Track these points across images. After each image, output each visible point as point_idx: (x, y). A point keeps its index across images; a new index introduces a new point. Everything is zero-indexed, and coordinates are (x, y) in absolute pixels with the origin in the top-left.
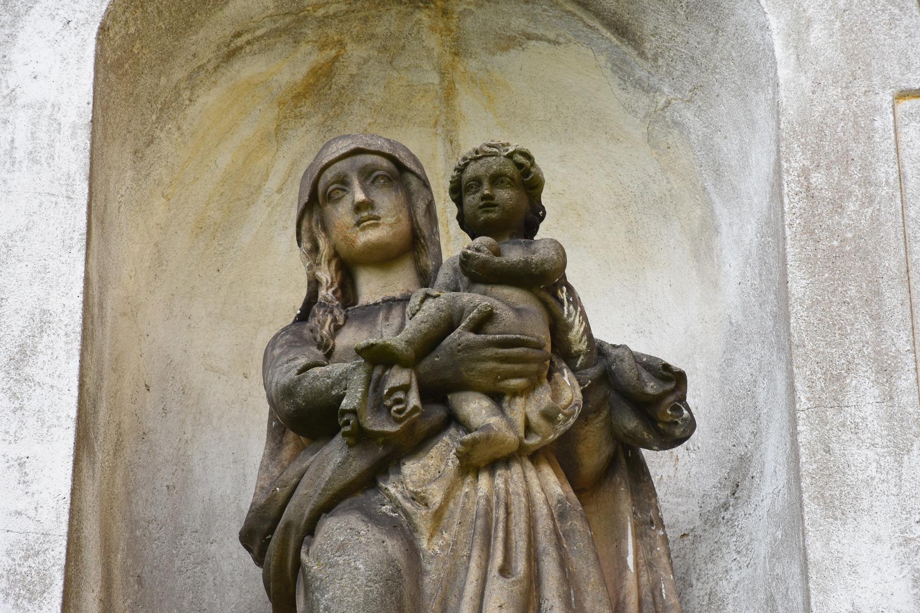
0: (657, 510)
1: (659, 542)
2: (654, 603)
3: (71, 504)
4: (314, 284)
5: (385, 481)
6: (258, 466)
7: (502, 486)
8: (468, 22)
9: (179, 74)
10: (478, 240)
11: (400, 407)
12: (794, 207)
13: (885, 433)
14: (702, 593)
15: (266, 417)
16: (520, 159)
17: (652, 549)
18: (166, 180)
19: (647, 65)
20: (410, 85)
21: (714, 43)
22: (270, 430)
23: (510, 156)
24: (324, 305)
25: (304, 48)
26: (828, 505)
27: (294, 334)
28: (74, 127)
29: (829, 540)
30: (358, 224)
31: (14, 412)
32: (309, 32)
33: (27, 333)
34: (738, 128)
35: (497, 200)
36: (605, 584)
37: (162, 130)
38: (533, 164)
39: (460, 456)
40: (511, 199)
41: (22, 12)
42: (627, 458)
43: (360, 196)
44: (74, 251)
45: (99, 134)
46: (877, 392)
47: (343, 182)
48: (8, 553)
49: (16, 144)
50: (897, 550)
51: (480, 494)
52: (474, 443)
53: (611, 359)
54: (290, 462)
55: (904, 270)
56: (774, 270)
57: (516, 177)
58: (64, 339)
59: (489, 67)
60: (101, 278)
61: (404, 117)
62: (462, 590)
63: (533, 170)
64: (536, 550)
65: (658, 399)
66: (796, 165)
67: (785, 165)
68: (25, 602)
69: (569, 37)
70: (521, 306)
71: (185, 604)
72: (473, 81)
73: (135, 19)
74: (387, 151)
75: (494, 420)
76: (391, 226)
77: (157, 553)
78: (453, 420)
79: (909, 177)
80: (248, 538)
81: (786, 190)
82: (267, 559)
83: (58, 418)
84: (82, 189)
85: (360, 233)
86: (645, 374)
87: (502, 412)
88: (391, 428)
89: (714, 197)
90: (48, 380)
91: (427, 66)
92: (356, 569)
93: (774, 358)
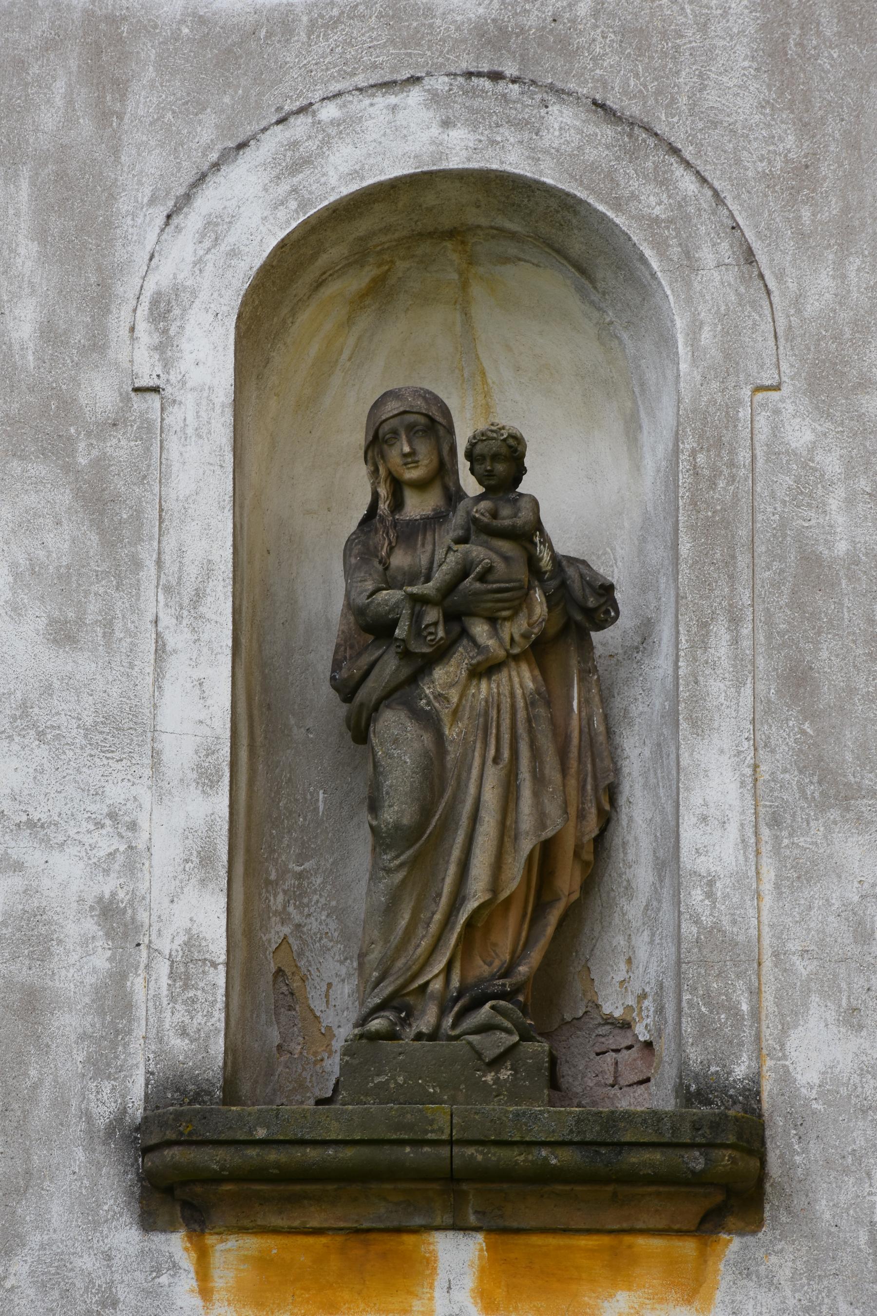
1: (594, 686)
7: (495, 690)
12: (685, 482)
13: (731, 669)
16: (511, 442)
17: (589, 691)
23: (505, 440)
26: (694, 724)
28: (223, 406)
29: (693, 751)
31: (194, 643)
33: (200, 579)
41: (187, 306)
44: (226, 510)
46: (728, 637)
47: (395, 433)
48: (196, 752)
49: (187, 422)
50: (733, 759)
58: (222, 583)
65: (595, 610)
66: (687, 446)
67: (681, 446)
70: (510, 554)
74: (424, 411)
78: (464, 633)
79: (759, 458)
84: (229, 458)
85: (406, 471)
88: (426, 650)
90: (214, 617)
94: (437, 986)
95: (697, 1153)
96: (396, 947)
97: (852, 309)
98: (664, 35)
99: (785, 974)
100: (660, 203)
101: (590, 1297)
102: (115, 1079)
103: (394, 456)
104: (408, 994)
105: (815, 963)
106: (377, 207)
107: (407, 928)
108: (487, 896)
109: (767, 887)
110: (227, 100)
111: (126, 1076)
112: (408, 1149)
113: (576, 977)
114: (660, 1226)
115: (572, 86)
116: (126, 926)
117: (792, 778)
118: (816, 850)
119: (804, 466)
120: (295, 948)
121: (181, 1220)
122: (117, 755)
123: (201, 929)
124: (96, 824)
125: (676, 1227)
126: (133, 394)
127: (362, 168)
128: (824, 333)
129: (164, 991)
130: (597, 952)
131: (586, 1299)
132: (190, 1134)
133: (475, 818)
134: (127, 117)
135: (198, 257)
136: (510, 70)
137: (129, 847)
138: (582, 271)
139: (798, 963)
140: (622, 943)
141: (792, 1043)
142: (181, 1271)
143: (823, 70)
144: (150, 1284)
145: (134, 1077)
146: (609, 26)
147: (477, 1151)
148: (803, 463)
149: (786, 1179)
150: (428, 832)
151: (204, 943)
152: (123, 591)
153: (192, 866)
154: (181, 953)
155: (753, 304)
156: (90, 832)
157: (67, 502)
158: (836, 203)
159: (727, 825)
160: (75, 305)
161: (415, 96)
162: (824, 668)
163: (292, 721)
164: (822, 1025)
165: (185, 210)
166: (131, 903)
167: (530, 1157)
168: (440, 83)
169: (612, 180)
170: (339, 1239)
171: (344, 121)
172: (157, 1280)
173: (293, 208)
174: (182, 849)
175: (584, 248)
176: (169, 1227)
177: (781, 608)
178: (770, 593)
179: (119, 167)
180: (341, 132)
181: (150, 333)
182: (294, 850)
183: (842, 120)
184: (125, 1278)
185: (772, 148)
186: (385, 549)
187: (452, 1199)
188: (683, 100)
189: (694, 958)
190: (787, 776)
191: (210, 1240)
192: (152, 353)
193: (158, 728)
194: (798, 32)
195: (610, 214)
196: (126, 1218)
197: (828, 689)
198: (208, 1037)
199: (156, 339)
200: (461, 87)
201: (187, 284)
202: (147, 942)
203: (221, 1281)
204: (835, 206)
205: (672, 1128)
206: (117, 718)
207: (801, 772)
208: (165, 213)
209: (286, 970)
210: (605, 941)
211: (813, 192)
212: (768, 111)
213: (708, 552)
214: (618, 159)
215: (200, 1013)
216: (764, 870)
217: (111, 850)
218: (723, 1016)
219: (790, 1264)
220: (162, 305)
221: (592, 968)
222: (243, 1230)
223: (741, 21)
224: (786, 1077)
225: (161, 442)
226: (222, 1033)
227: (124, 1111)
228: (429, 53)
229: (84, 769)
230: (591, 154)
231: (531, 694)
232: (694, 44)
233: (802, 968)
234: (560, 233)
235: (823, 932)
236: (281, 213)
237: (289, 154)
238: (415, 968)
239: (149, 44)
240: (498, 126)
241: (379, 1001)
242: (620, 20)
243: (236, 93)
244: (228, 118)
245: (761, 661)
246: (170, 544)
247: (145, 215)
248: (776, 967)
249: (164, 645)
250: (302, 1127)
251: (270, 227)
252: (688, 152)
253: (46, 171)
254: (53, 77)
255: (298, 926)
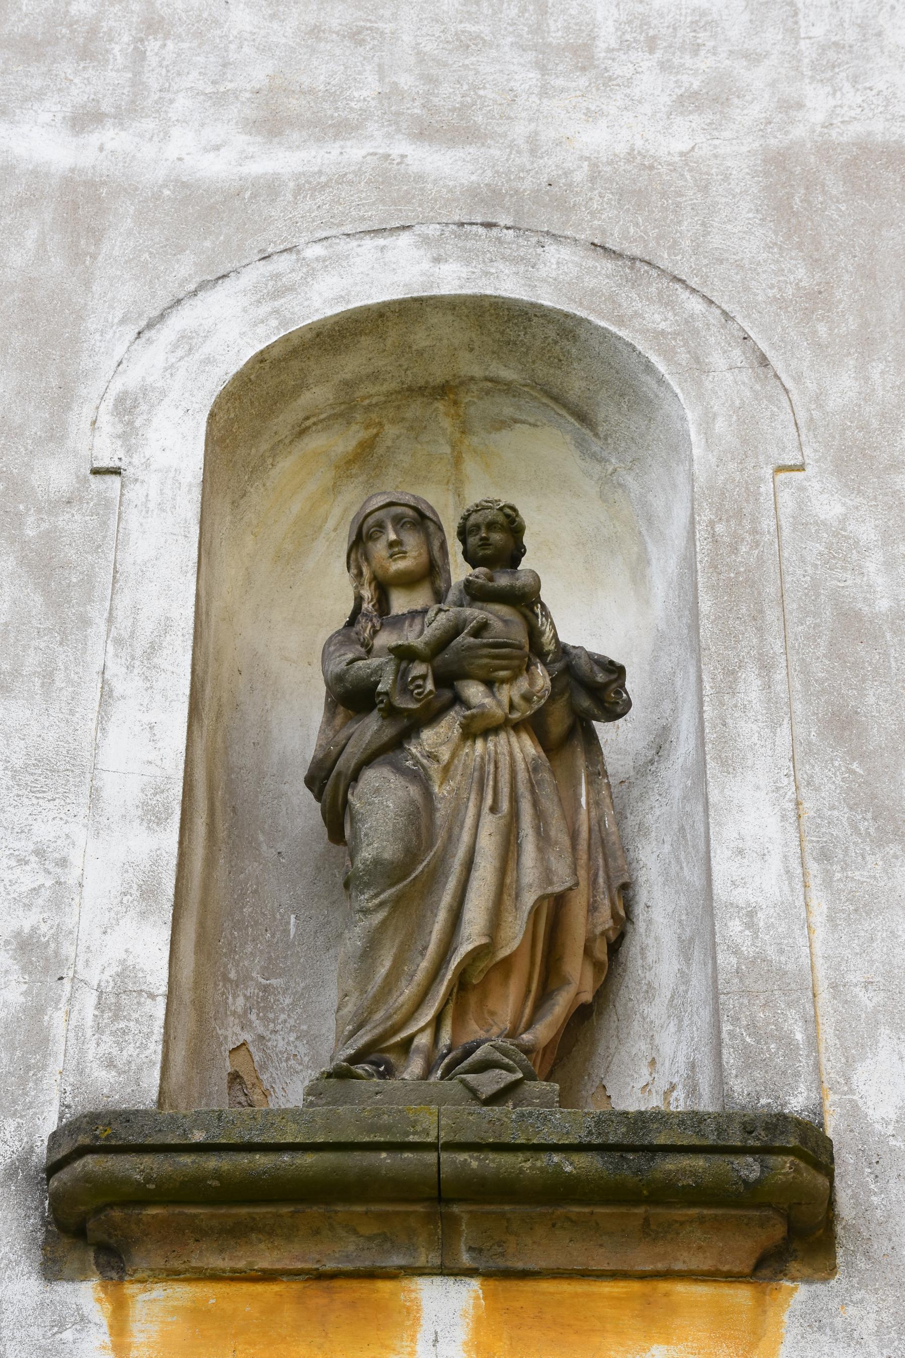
0: (603, 765)
1: (604, 788)
2: (600, 831)
3: (186, 756)
4: (359, 599)
5: (409, 743)
6: (318, 729)
8: (472, 410)
9: (264, 446)
10: (477, 570)
11: (420, 690)
13: (764, 712)
14: (634, 823)
15: (324, 694)
17: (599, 792)
18: (255, 522)
19: (600, 443)
20: (429, 455)
21: (648, 429)
22: (327, 704)
23: (501, 509)
24: (366, 615)
25: (355, 427)
26: (724, 763)
27: (344, 635)
28: (190, 485)
29: (724, 788)
30: (391, 556)
31: (146, 690)
32: (358, 416)
33: (156, 633)
34: (665, 490)
35: (491, 541)
36: (565, 818)
37: (252, 487)
38: (517, 515)
39: (462, 726)
40: (501, 540)
41: (156, 403)
42: (582, 725)
43: (393, 536)
44: (189, 575)
45: (208, 490)
46: (759, 683)
47: (381, 526)
48: (143, 790)
49: (150, 498)
50: (771, 795)
51: (477, 754)
52: (473, 717)
53: (572, 657)
54: (341, 728)
55: (780, 595)
56: (689, 593)
57: (505, 524)
58: (181, 638)
59: (487, 442)
60: (207, 593)
61: (425, 477)
62: (463, 822)
63: (517, 519)
64: (516, 794)
65: (606, 686)
66: (705, 518)
67: (697, 518)
68: (155, 825)
69: (545, 421)
70: (508, 618)
71: (266, 826)
72: (475, 452)
73: (235, 408)
75: (487, 701)
76: (415, 558)
77: (246, 791)
78: (458, 700)
79: (784, 528)
80: (310, 782)
81: (698, 536)
82: (324, 797)
83: (177, 695)
86: (596, 668)
87: (493, 695)
88: (413, 706)
89: (647, 538)
90: (170, 668)
91: (442, 441)
92: (387, 806)
93: (688, 656)
94: (423, 1041)
95: (750, 1160)
96: (374, 997)
97: (878, 404)
98: (664, 195)
99: (846, 1006)
100: (666, 320)
101: (617, 1352)
102: (21, 1117)
103: (379, 549)
104: (388, 1049)
105: (882, 994)
106: (365, 341)
107: (388, 976)
108: (484, 940)
109: (819, 917)
110: (207, 244)
111: (35, 1114)
112: (384, 1155)
113: (589, 1100)
114: (705, 1267)
115: (568, 233)
116: (47, 959)
117: (843, 814)
118: (875, 883)
119: (836, 534)
120: (256, 1058)
121: (94, 1267)
122: (49, 795)
123: (138, 961)
124: (18, 861)
125: (726, 1268)
126: (91, 477)
127: (348, 294)
128: (849, 424)
129: (89, 1022)
130: (614, 1068)
131: (612, 1353)
132: (108, 1138)
133: (469, 865)
134: (100, 258)
135: (170, 363)
136: (504, 220)
137: (57, 882)
138: (582, 417)
139: (861, 994)
140: (643, 1048)
141: (861, 1074)
142: (90, 1325)
143: (831, 219)
144: (49, 1341)
145: (45, 1114)
146: (606, 189)
147: (471, 1157)
148: (834, 532)
149: (862, 1221)
150: (414, 875)
151: (140, 975)
152: (68, 646)
153: (131, 899)
154: (112, 984)
155: (770, 399)
156: (12, 868)
157: (10, 568)
158: (854, 320)
159: (766, 858)
160: (33, 404)
161: (405, 239)
162: (872, 712)
163: (261, 838)
164: (895, 1058)
165: (158, 326)
166: (55, 938)
167: (539, 1164)
168: (432, 230)
169: (614, 302)
170: (296, 1287)
171: (330, 258)
172: (59, 1336)
173: (274, 325)
174: (120, 882)
175: (584, 384)
176: (81, 1275)
177: (818, 658)
178: (805, 645)
179: (90, 295)
180: (326, 266)
181: (113, 424)
182: (259, 962)
183: (855, 257)
184: (18, 1334)
185: (782, 278)
186: (368, 631)
187: (439, 1231)
188: (686, 243)
189: (735, 988)
190: (836, 813)
191: (130, 1288)
192: (114, 440)
193: (99, 766)
194: (803, 191)
195: (613, 329)
196: (24, 1267)
197: (878, 731)
198: (140, 1069)
199: (120, 429)
200: (453, 232)
201: (157, 385)
202: (71, 974)
203: (141, 1335)
204: (853, 323)
205: (717, 1130)
206: (52, 760)
207: (851, 809)
208: (137, 331)
209: (246, 1078)
210: (623, 1054)
211: (828, 311)
212: (776, 250)
213: (732, 608)
214: (619, 285)
215: (132, 1045)
216: (814, 903)
217: (36, 885)
218: (773, 1046)
219: (873, 1316)
220: (128, 402)
221: (608, 1085)
222: (173, 1275)
223: (743, 184)
224: (854, 1112)
225: (120, 514)
226: (158, 1066)
227: (31, 1150)
228: (420, 209)
229: (9, 809)
230: (590, 282)
231: (533, 759)
232: (695, 201)
233: (867, 1000)
234: (558, 372)
235: (890, 963)
236: (261, 330)
237: (271, 283)
238: (396, 1018)
239: (128, 203)
240: (491, 261)
241: (352, 1052)
242: (617, 184)
243: (217, 239)
244: (208, 258)
245: (798, 707)
246: (124, 602)
247: (115, 332)
248: (835, 998)
249: (111, 691)
250: (251, 1129)
251: (248, 340)
252: (694, 282)
253: (11, 298)
254: (25, 226)
255: (261, 1038)
